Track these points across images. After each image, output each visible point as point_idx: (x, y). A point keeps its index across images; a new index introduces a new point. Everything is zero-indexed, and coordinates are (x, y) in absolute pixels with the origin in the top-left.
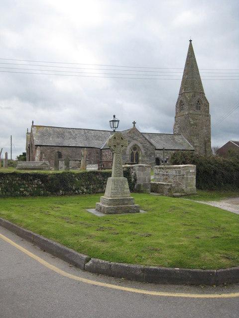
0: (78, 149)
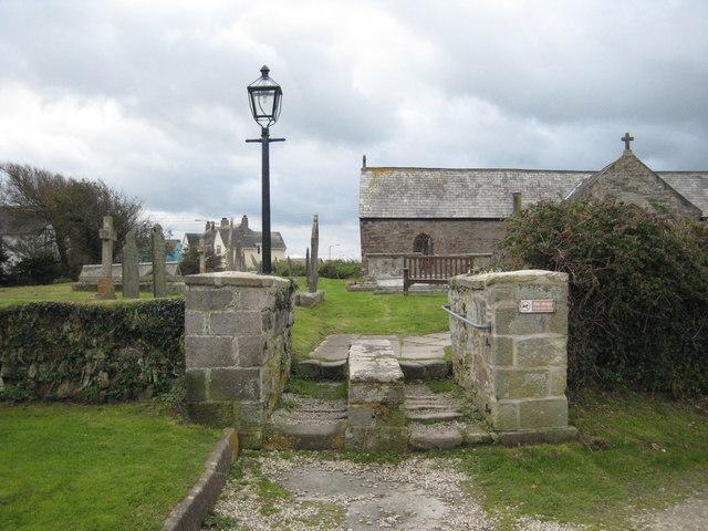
0: (477, 225)
